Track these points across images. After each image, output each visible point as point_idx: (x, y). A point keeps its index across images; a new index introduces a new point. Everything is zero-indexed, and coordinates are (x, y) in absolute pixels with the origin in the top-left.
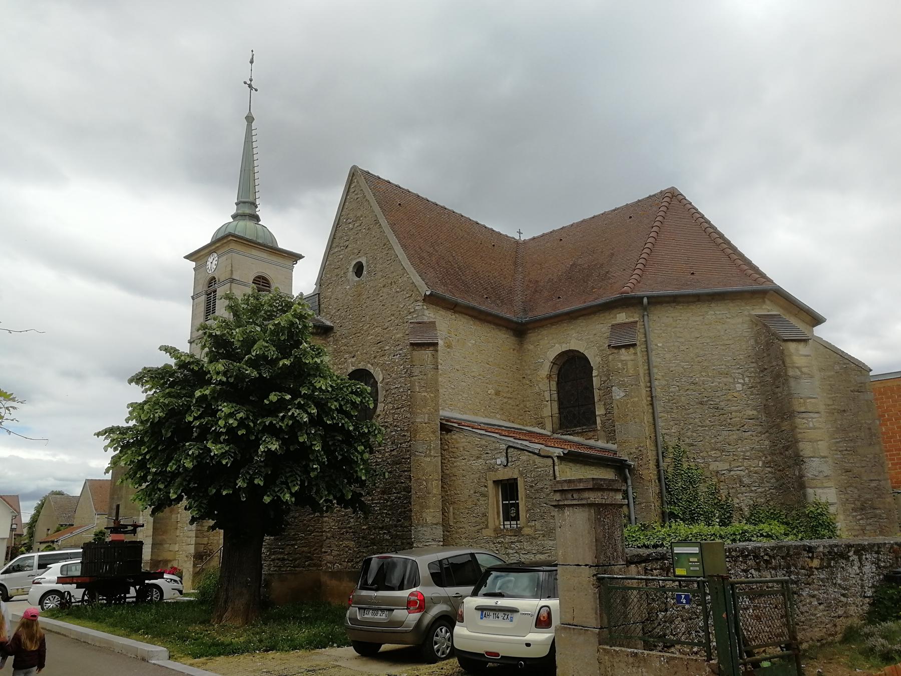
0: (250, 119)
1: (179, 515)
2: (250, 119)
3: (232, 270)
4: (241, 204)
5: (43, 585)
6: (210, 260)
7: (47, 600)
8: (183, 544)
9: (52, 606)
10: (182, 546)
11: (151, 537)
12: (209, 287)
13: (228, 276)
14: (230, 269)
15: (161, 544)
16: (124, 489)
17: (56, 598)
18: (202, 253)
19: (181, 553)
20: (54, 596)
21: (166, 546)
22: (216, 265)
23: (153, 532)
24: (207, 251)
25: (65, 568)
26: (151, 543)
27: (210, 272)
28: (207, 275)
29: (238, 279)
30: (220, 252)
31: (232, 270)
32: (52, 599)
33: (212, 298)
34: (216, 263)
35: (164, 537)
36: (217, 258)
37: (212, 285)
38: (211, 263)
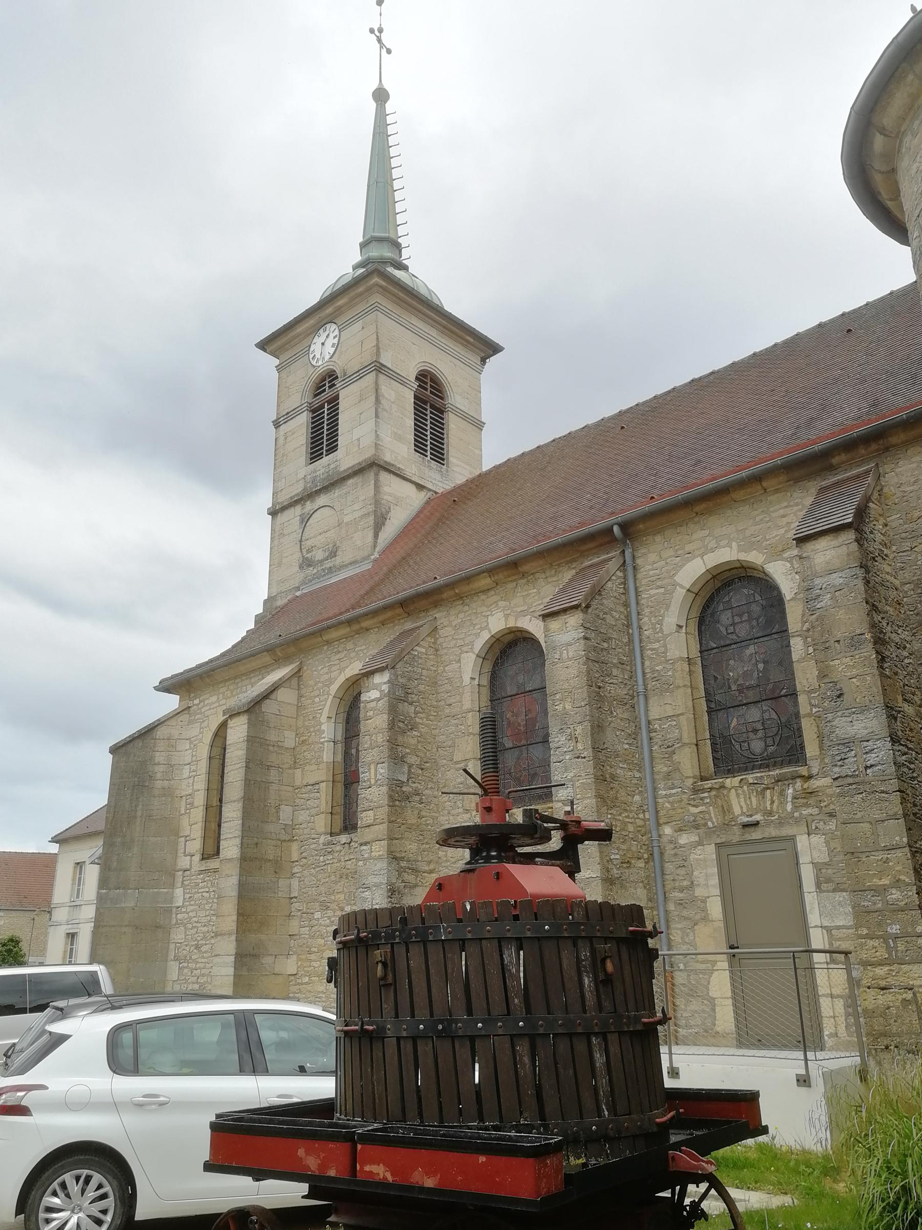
0: (381, 96)
1: (295, 883)
2: (381, 96)
3: (377, 346)
4: (374, 243)
5: (36, 1119)
6: (318, 340)
7: (55, 1194)
8: (313, 957)
9: (74, 1220)
10: (311, 961)
11: (233, 937)
12: (316, 395)
13: (367, 358)
14: (374, 344)
15: (256, 956)
16: (138, 819)
17: (93, 1184)
18: (300, 329)
19: (306, 979)
20: (85, 1172)
21: (267, 960)
22: (337, 347)
23: (239, 923)
24: (311, 322)
25: (127, 1037)
26: (233, 951)
27: (320, 363)
28: (311, 370)
29: (390, 367)
30: (340, 321)
31: (377, 346)
32: (74, 1188)
33: (326, 417)
34: (336, 341)
35: (263, 937)
36: (337, 332)
37: (324, 390)
38: (323, 344)
